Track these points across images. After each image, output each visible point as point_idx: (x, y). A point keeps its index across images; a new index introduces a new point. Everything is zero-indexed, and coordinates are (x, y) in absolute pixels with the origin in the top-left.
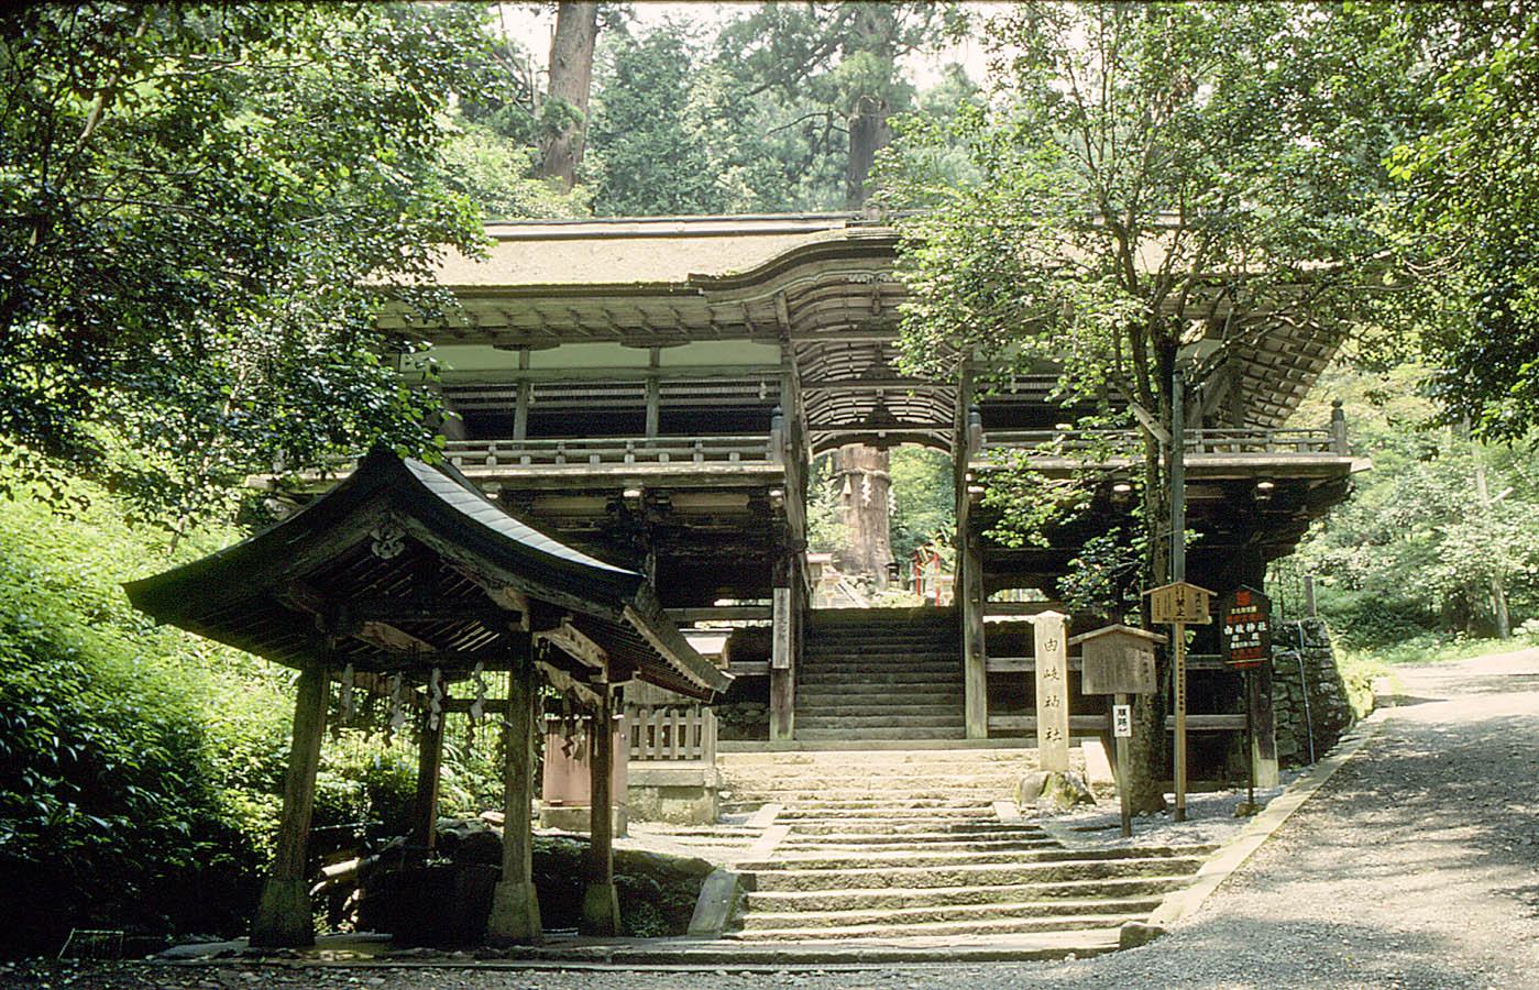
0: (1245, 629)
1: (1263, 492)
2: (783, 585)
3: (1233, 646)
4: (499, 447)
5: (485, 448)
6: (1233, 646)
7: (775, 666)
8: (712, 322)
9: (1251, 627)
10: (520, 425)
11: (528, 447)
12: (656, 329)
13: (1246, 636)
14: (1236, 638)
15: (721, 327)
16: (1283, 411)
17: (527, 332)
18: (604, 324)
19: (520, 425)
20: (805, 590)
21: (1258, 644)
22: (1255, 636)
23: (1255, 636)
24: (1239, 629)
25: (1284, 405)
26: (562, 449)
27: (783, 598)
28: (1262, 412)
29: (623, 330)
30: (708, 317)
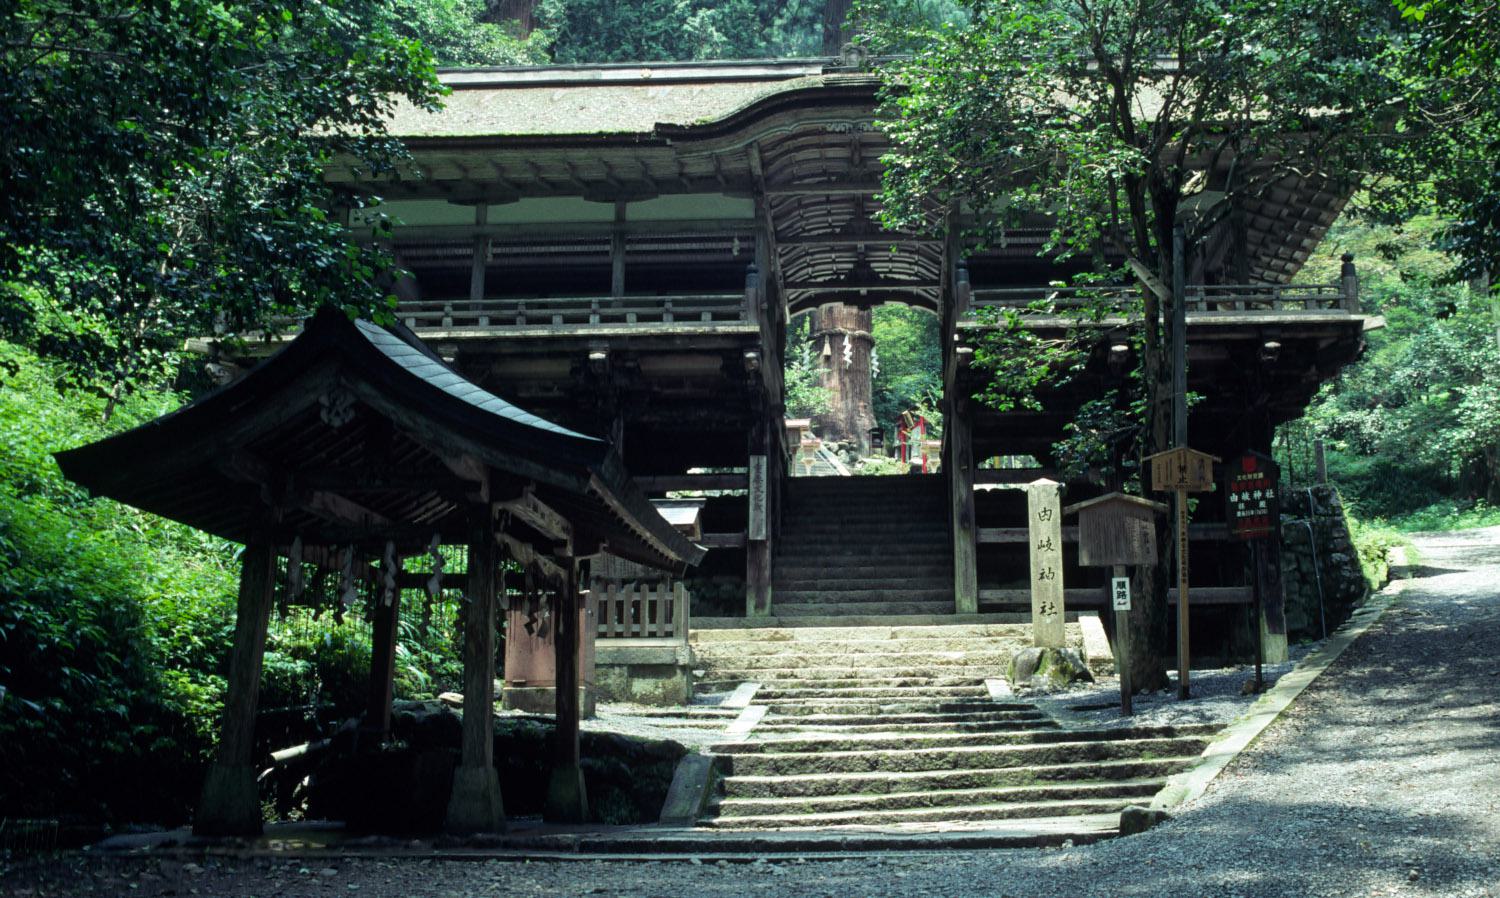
0: (1251, 496)
1: (1271, 351)
2: (759, 452)
3: (1239, 514)
4: (456, 308)
5: (441, 308)
6: (1239, 514)
7: (751, 537)
8: (681, 174)
9: (1258, 494)
10: (477, 283)
11: (486, 307)
12: (622, 182)
13: (1252, 504)
14: (1242, 506)
15: (692, 179)
16: (1290, 266)
17: (483, 185)
18: (566, 177)
19: (477, 283)
20: (782, 455)
21: (1265, 512)
22: (1262, 504)
23: (1262, 504)
24: (1246, 496)
25: (1292, 260)
26: (522, 309)
27: (759, 466)
28: (1268, 267)
29: (588, 183)
30: (675, 169)
